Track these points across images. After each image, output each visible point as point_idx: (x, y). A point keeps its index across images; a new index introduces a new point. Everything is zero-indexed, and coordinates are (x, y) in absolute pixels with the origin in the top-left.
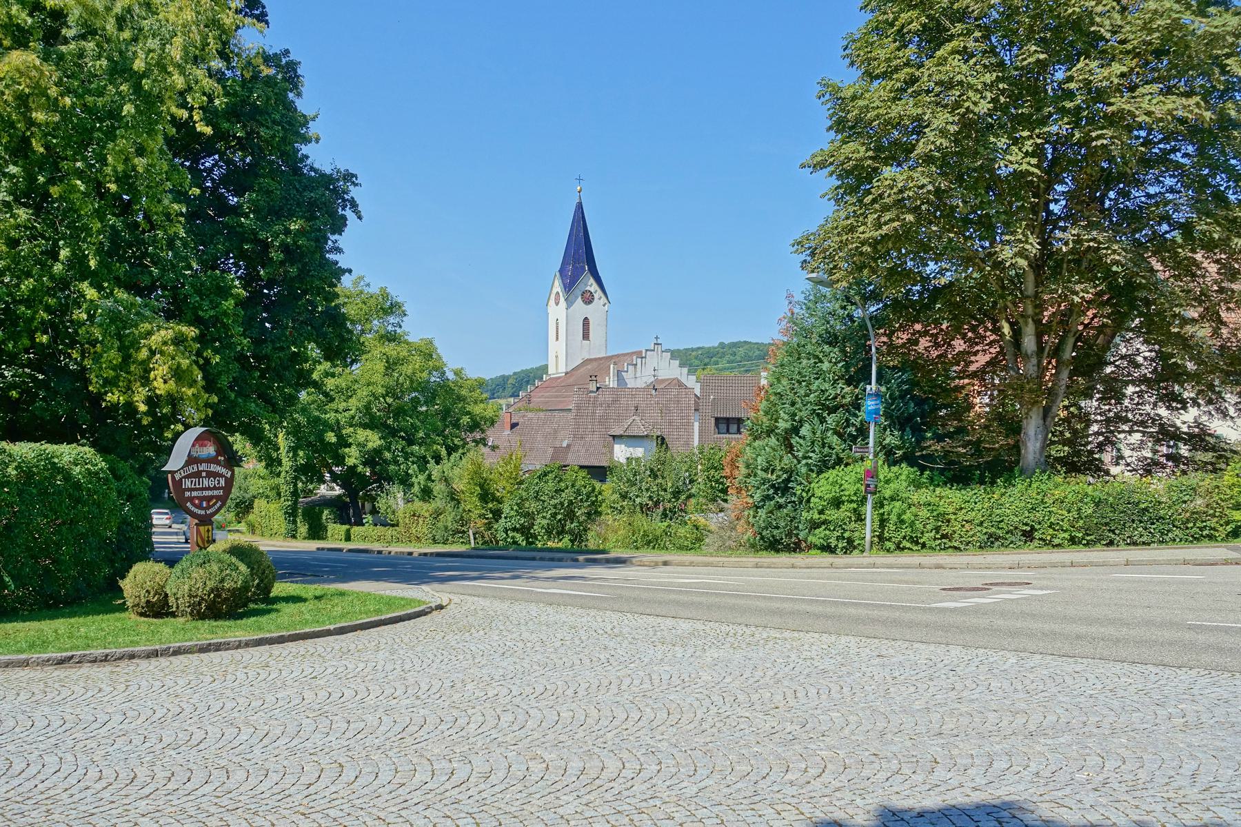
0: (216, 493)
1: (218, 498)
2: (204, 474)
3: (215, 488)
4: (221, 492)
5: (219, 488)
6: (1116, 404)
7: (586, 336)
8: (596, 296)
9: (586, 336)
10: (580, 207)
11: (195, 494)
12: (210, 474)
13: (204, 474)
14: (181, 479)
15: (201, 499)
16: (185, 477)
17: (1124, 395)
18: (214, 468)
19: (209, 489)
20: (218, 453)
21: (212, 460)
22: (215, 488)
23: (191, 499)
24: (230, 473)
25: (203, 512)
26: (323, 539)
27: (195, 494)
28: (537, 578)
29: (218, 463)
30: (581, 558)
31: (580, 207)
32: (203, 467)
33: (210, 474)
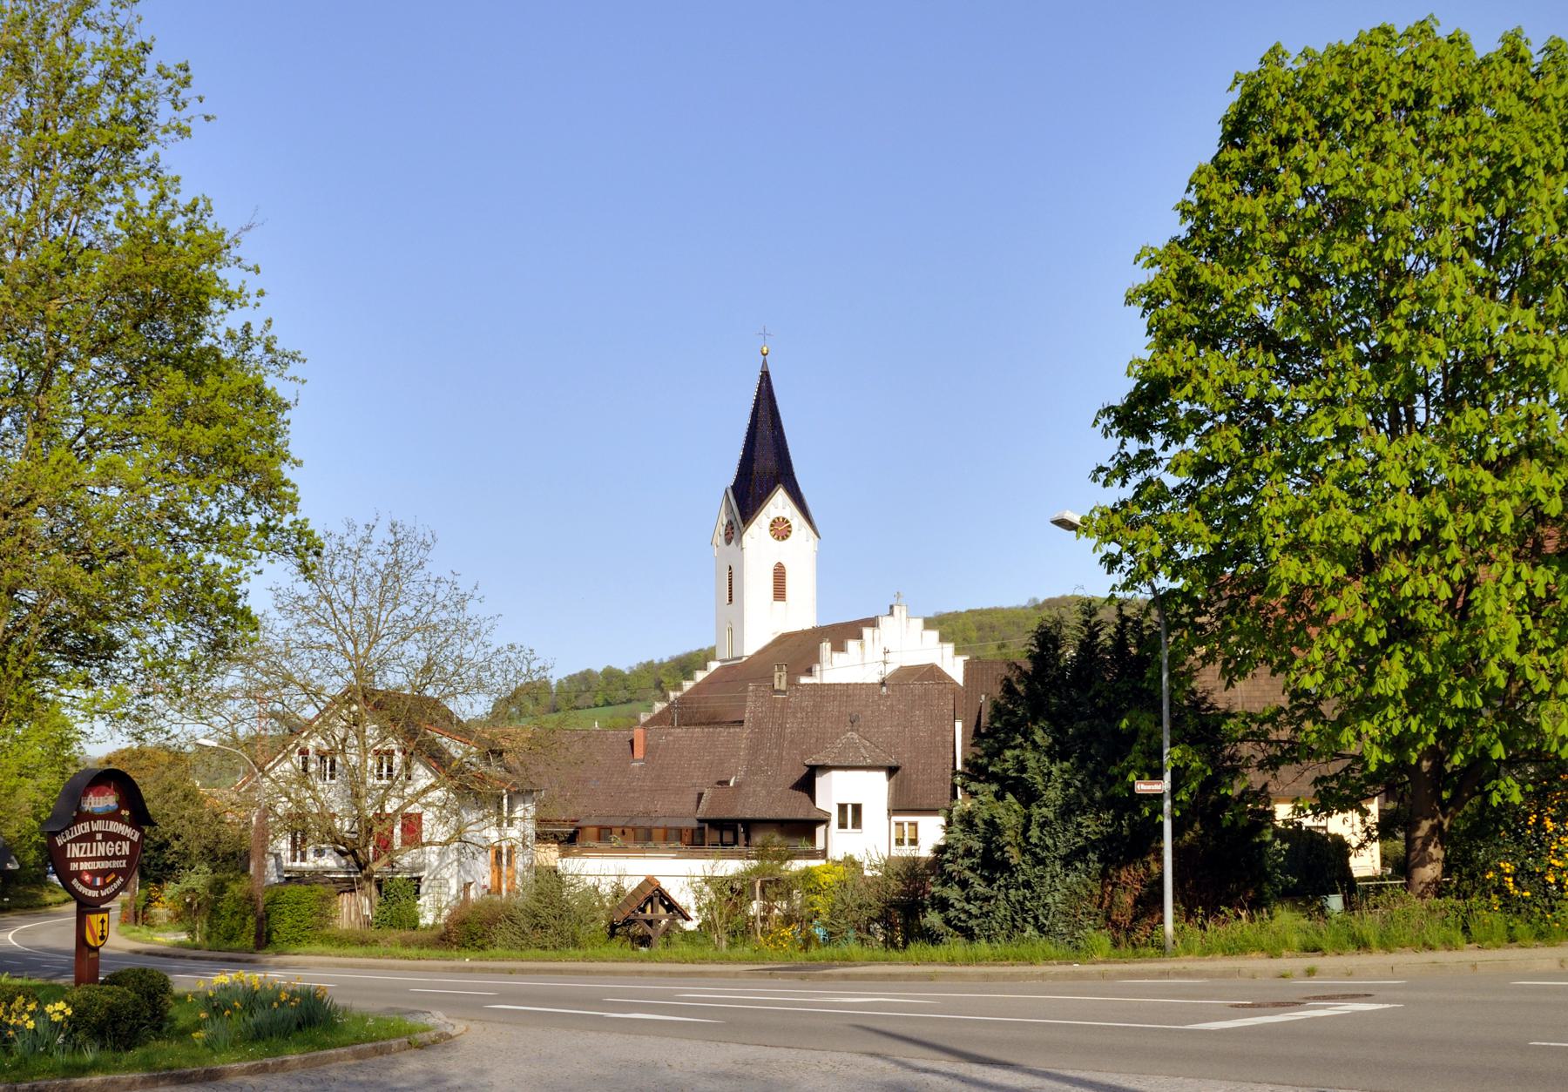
0: (116, 864)
1: (118, 872)
2: (99, 837)
3: (115, 857)
4: (123, 864)
5: (121, 858)
6: (1341, 527)
7: (779, 593)
8: (773, 516)
9: (779, 593)
10: (765, 377)
11: (85, 866)
12: (109, 837)
13: (99, 837)
14: (65, 844)
15: (94, 873)
16: (71, 841)
17: (1385, 281)
18: (116, 827)
19: (106, 858)
20: (121, 804)
21: (113, 816)
22: (115, 857)
23: (78, 874)
24: (137, 835)
25: (94, 894)
26: (708, 880)
27: (85, 866)
28: (827, 976)
29: (120, 819)
30: (394, 1043)
31: (765, 377)
32: (98, 826)
33: (109, 837)
